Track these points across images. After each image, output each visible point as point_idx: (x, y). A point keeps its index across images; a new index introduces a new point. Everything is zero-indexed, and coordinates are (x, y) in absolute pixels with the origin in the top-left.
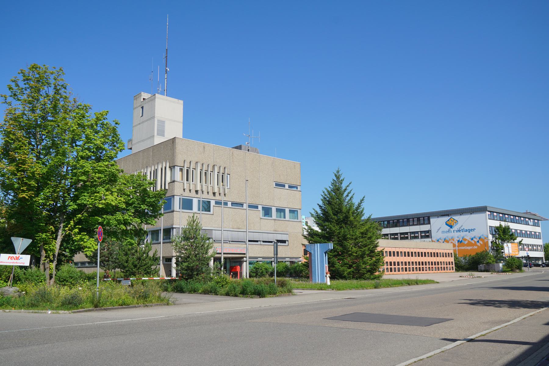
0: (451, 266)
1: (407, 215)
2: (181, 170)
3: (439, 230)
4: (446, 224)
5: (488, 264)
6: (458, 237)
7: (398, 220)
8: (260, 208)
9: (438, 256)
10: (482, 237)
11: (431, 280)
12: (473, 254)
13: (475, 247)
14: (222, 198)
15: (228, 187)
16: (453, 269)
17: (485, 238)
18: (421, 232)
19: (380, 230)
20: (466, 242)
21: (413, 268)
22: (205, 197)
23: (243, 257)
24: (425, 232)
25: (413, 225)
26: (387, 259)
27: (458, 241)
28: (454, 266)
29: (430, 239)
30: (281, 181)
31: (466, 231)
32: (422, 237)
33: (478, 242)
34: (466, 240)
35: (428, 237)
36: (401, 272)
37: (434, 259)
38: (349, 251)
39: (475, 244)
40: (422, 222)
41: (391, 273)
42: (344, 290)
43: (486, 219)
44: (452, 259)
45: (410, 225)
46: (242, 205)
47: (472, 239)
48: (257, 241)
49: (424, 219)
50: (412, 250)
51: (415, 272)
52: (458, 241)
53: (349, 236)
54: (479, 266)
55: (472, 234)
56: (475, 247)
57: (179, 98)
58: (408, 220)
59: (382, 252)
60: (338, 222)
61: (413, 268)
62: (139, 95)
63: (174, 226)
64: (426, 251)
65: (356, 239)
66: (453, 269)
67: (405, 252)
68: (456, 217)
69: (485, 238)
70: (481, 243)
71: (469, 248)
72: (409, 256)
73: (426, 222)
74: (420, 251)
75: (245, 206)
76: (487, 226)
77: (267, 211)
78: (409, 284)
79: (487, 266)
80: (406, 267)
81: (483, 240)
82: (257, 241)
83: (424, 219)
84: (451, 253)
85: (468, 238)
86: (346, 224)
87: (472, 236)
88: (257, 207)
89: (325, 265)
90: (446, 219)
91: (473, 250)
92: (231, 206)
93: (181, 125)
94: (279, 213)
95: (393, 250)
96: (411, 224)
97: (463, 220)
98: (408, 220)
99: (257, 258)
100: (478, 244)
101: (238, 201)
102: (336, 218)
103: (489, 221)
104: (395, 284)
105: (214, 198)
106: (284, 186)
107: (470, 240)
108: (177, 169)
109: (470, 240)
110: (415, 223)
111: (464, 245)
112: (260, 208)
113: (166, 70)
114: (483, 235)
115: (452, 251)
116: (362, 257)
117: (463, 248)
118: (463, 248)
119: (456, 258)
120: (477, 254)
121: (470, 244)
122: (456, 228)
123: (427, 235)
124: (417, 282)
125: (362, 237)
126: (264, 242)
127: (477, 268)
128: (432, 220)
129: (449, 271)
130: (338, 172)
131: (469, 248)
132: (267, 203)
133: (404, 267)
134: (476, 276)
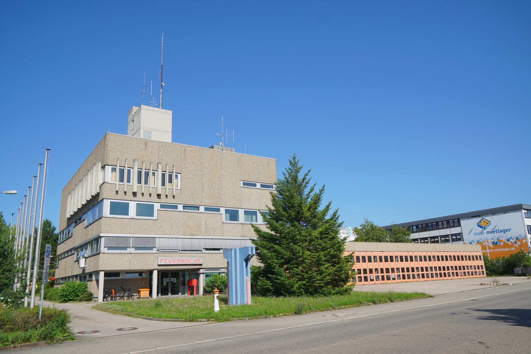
0: (481, 270)
1: (436, 219)
2: (114, 170)
3: (470, 232)
4: (478, 226)
5: (526, 266)
6: (492, 239)
7: (427, 224)
8: (222, 211)
9: (463, 260)
10: (519, 237)
11: (422, 294)
12: (507, 256)
13: (513, 249)
14: (170, 201)
15: (179, 188)
16: (483, 274)
17: (523, 239)
18: (451, 235)
19: (409, 235)
20: (502, 244)
21: (432, 274)
22: (146, 200)
23: (199, 269)
24: (456, 235)
25: (443, 228)
26: (357, 266)
27: (493, 243)
28: (484, 270)
29: (461, 243)
30: (251, 179)
31: (501, 231)
32: (453, 240)
33: (515, 242)
34: (501, 241)
35: (460, 240)
36: (416, 279)
37: (424, 264)
38: (300, 257)
39: (512, 245)
40: (452, 224)
41: (404, 280)
42: (227, 320)
43: (523, 218)
44: (481, 263)
45: (439, 229)
46: (198, 208)
47: (508, 240)
48: (219, 249)
49: (453, 221)
50: (429, 254)
51: (435, 278)
52: (493, 243)
53: (298, 237)
54: (515, 270)
55: (508, 235)
56: (513, 249)
57: (165, 107)
58: (437, 223)
59: (351, 256)
60: (291, 220)
61: (432, 274)
62: (131, 109)
63: (101, 235)
64: (448, 254)
65: (312, 240)
66: (483, 274)
67: (454, 256)
68: (488, 218)
69: (523, 239)
70: (519, 243)
71: (506, 250)
72: (459, 260)
73: (456, 224)
74: (440, 254)
75: (202, 209)
76: (524, 225)
77: (233, 215)
78: (374, 303)
79: (524, 270)
80: (385, 275)
81: (521, 241)
82: (219, 249)
83: (454, 222)
84: (480, 256)
85: (503, 239)
86: (299, 221)
87: (509, 237)
88: (218, 210)
89: (245, 277)
90: (478, 220)
91: (506, 252)
92: (182, 210)
93: (171, 135)
94: (250, 216)
95: (406, 254)
96: (440, 227)
97: (495, 220)
98: (437, 223)
99: (218, 269)
100: (516, 245)
101: (192, 203)
102: (286, 215)
103: (526, 220)
104: (345, 304)
105: (158, 200)
106: (255, 185)
107: (506, 241)
108: (108, 169)
109: (506, 241)
110: (445, 227)
111: (500, 247)
112: (222, 211)
113: (162, 85)
114: (520, 236)
115: (481, 254)
116: (318, 263)
117: (499, 250)
118: (499, 250)
119: (485, 259)
120: (511, 256)
121: (506, 245)
122: (489, 229)
123: (458, 238)
124: (390, 298)
125: (321, 239)
126: (207, 249)
127: (513, 272)
128: (462, 222)
129: (478, 276)
130: (294, 158)
131: (506, 250)
132: (232, 205)
133: (420, 273)
134: (501, 283)
